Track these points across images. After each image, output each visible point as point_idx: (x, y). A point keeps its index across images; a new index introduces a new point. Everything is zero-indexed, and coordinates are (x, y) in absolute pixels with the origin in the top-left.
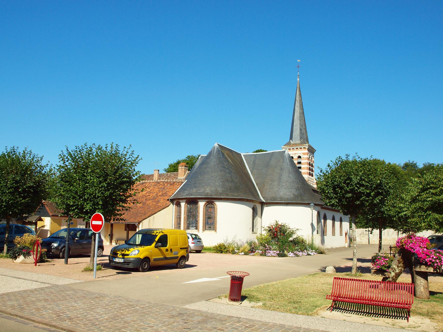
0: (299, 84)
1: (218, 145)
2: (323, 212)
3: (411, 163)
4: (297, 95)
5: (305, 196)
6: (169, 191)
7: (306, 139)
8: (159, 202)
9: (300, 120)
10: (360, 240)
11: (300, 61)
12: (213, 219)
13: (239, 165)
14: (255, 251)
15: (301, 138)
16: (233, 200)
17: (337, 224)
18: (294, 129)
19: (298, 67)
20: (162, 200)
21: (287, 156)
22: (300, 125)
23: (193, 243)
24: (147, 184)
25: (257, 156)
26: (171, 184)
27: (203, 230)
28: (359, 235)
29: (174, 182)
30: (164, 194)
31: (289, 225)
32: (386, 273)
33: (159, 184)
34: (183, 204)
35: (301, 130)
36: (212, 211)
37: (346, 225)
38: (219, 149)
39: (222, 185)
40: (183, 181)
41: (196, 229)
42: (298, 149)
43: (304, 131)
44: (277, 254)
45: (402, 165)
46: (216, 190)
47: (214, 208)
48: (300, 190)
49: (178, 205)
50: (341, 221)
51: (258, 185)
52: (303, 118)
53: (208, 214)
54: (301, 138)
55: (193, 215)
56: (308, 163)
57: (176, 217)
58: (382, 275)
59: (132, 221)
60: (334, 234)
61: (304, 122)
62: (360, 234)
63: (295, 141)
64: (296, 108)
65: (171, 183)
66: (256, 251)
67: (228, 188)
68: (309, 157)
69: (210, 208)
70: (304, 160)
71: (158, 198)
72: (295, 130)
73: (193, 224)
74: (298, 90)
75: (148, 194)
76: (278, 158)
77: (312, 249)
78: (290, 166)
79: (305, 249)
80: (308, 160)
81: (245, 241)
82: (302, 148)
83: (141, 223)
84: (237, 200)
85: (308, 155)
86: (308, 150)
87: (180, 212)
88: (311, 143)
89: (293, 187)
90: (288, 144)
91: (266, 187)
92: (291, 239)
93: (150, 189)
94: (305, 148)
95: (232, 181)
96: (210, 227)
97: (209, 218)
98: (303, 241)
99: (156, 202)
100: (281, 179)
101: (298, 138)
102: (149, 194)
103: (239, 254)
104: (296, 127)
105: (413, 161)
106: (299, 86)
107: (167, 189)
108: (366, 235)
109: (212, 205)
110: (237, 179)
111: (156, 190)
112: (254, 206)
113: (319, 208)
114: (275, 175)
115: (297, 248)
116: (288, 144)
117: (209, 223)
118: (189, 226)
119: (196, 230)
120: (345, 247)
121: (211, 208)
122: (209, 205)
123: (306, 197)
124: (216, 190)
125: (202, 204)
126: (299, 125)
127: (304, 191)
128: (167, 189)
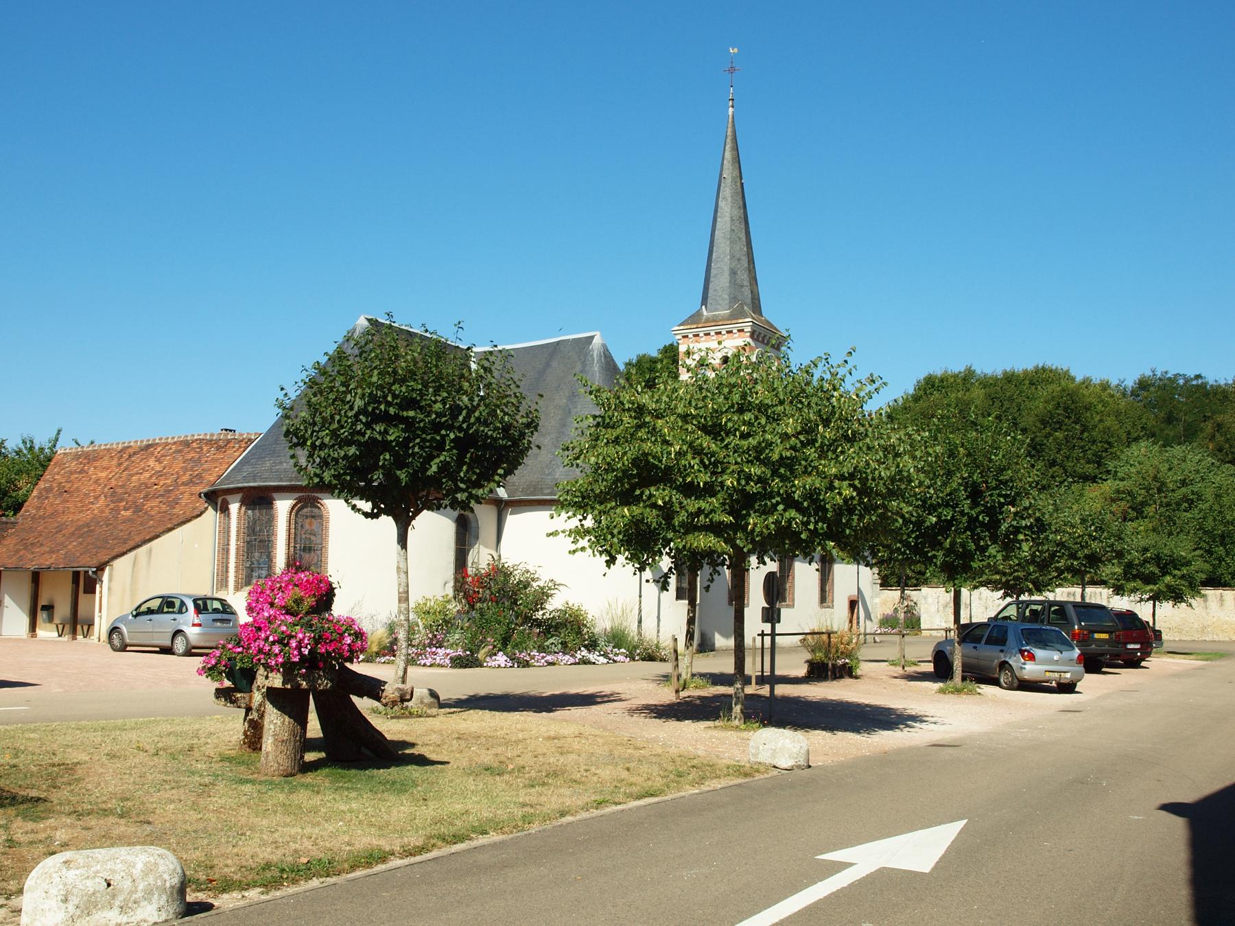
0: (733, 126)
3: (1160, 379)
6: (209, 470)
7: (749, 301)
8: (177, 503)
9: (731, 242)
11: (736, 50)
12: (319, 553)
15: (734, 298)
19: (732, 70)
20: (187, 495)
22: (731, 259)
23: (200, 625)
24: (159, 449)
26: (219, 448)
28: (941, 608)
29: (229, 441)
32: (239, 695)
33: (189, 446)
34: (234, 508)
35: (733, 273)
36: (314, 527)
40: (253, 437)
43: (743, 277)
45: (1130, 383)
47: (321, 517)
49: (224, 509)
52: (743, 236)
54: (734, 299)
55: (260, 541)
57: (223, 549)
58: (226, 700)
59: (81, 563)
63: (716, 310)
65: (221, 443)
69: (308, 521)
71: (178, 490)
72: (716, 276)
73: (262, 568)
74: (728, 147)
75: (154, 480)
76: (569, 359)
82: (735, 331)
87: (226, 531)
88: (773, 313)
90: (695, 319)
93: (162, 463)
94: (742, 330)
99: (170, 502)
101: (724, 299)
102: (157, 478)
105: (1166, 373)
106: (734, 132)
107: (206, 461)
109: (316, 510)
111: (178, 465)
116: (695, 319)
121: (313, 517)
122: (305, 510)
125: (283, 506)
128: (206, 461)
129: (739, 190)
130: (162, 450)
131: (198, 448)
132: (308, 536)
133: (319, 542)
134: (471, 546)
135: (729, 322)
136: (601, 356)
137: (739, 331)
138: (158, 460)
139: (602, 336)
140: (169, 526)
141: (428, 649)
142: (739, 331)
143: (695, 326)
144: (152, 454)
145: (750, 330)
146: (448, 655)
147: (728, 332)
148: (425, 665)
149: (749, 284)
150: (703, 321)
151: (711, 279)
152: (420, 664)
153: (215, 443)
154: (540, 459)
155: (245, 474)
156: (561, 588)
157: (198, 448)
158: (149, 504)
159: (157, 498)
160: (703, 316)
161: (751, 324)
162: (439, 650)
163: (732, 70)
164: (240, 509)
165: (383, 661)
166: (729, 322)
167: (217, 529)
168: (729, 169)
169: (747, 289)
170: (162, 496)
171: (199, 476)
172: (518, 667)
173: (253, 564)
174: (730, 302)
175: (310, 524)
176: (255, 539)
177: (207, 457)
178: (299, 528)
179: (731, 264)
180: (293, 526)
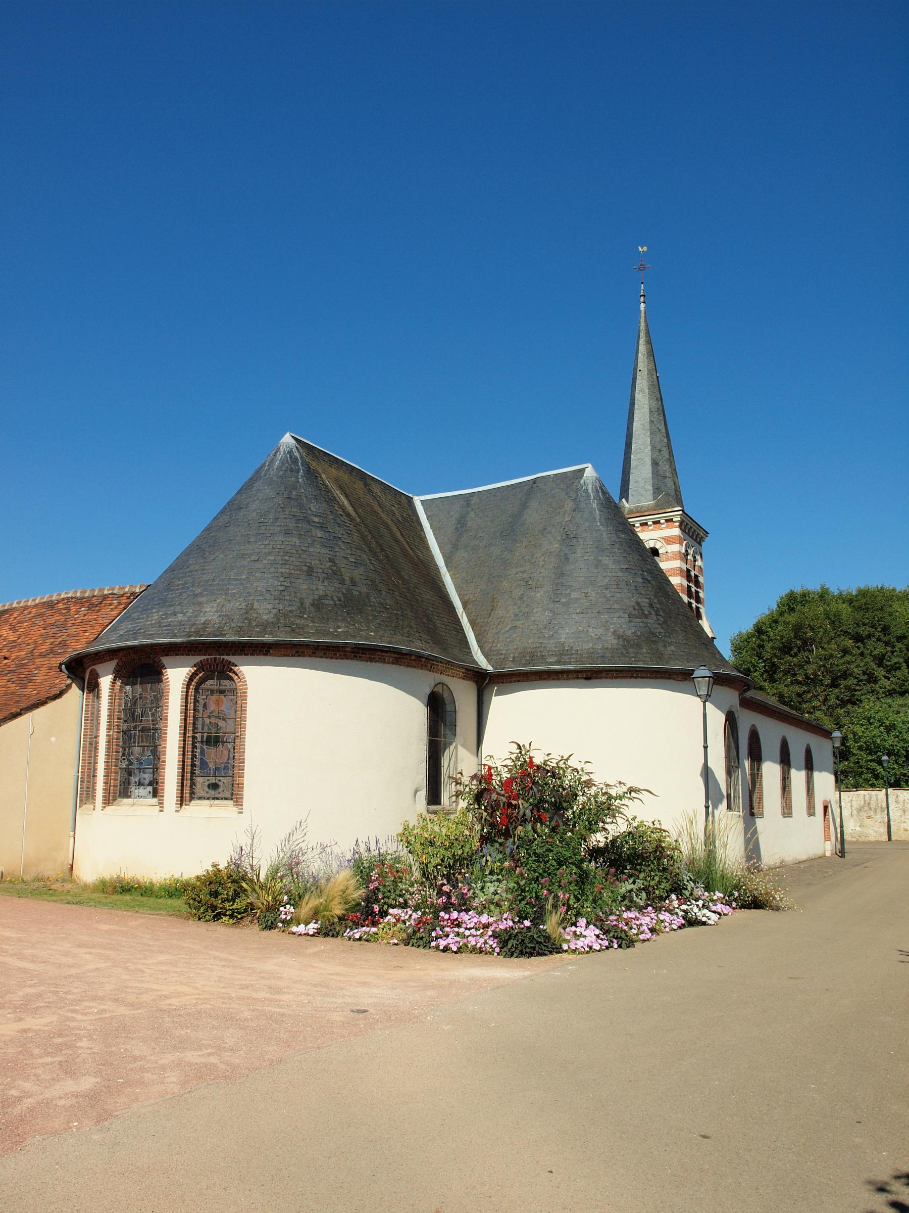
1: (293, 441)
2: (747, 720)
4: (640, 355)
5: (671, 644)
7: (672, 492)
8: (31, 681)
9: (651, 433)
10: (858, 829)
11: (645, 249)
12: (230, 746)
13: (394, 528)
14: (384, 914)
15: (658, 489)
16: (325, 656)
17: (798, 777)
18: (633, 463)
20: (43, 670)
21: (590, 487)
22: (652, 450)
25: (474, 500)
27: (181, 801)
28: (855, 812)
30: (56, 646)
31: (588, 769)
34: (105, 682)
35: (655, 463)
36: (223, 707)
37: (824, 781)
38: (297, 454)
39: (281, 588)
41: (155, 794)
42: (646, 524)
43: (665, 468)
44: (495, 935)
46: (250, 608)
47: (234, 691)
48: (646, 617)
49: (93, 687)
50: (809, 766)
51: (470, 606)
52: (662, 427)
53: (207, 721)
54: (657, 490)
55: (142, 730)
56: (681, 569)
57: (91, 744)
60: (787, 811)
61: (665, 440)
62: (860, 810)
64: (638, 396)
65: (94, 600)
66: (391, 911)
67: (307, 602)
68: (686, 551)
69: (214, 698)
70: (668, 560)
72: (636, 467)
77: (708, 888)
78: (602, 524)
79: (672, 891)
80: (681, 559)
81: (345, 849)
84: (346, 657)
85: (681, 544)
86: (680, 526)
87: (93, 718)
89: (616, 606)
91: (500, 612)
92: (598, 839)
94: (671, 520)
95: (335, 574)
96: (214, 786)
97: (214, 741)
98: (659, 851)
100: (562, 574)
101: (646, 490)
103: (294, 929)
104: (639, 456)
107: (73, 625)
108: (879, 811)
109: (226, 683)
110: (361, 570)
112: (439, 689)
113: (731, 697)
114: (541, 563)
115: (625, 887)
117: (212, 766)
118: (129, 784)
120: (824, 856)
121: (222, 692)
122: (209, 682)
123: (673, 648)
124: (250, 608)
127: (665, 622)
128: (73, 625)
129: (656, 382)
130: (19, 615)
131: (65, 609)
132: (213, 721)
133: (230, 729)
135: (656, 512)
136: (597, 491)
137: (667, 521)
138: (13, 629)
139: (595, 468)
140: (14, 710)
141: (442, 914)
142: (667, 521)
144: (7, 621)
146: (486, 926)
147: (654, 523)
148: (446, 949)
149: (671, 475)
151: (631, 471)
152: (437, 947)
153: (86, 602)
154: (533, 619)
155: (122, 633)
156: (644, 796)
157: (65, 609)
159: (6, 675)
160: (625, 508)
161: (681, 512)
162: (465, 917)
163: (642, 268)
164: (113, 683)
166: (656, 512)
167: (84, 715)
168: (644, 362)
169: (670, 480)
170: (12, 672)
171: (63, 644)
172: (620, 946)
174: (654, 493)
175: (218, 703)
176: (135, 727)
179: (652, 454)
180: (191, 706)
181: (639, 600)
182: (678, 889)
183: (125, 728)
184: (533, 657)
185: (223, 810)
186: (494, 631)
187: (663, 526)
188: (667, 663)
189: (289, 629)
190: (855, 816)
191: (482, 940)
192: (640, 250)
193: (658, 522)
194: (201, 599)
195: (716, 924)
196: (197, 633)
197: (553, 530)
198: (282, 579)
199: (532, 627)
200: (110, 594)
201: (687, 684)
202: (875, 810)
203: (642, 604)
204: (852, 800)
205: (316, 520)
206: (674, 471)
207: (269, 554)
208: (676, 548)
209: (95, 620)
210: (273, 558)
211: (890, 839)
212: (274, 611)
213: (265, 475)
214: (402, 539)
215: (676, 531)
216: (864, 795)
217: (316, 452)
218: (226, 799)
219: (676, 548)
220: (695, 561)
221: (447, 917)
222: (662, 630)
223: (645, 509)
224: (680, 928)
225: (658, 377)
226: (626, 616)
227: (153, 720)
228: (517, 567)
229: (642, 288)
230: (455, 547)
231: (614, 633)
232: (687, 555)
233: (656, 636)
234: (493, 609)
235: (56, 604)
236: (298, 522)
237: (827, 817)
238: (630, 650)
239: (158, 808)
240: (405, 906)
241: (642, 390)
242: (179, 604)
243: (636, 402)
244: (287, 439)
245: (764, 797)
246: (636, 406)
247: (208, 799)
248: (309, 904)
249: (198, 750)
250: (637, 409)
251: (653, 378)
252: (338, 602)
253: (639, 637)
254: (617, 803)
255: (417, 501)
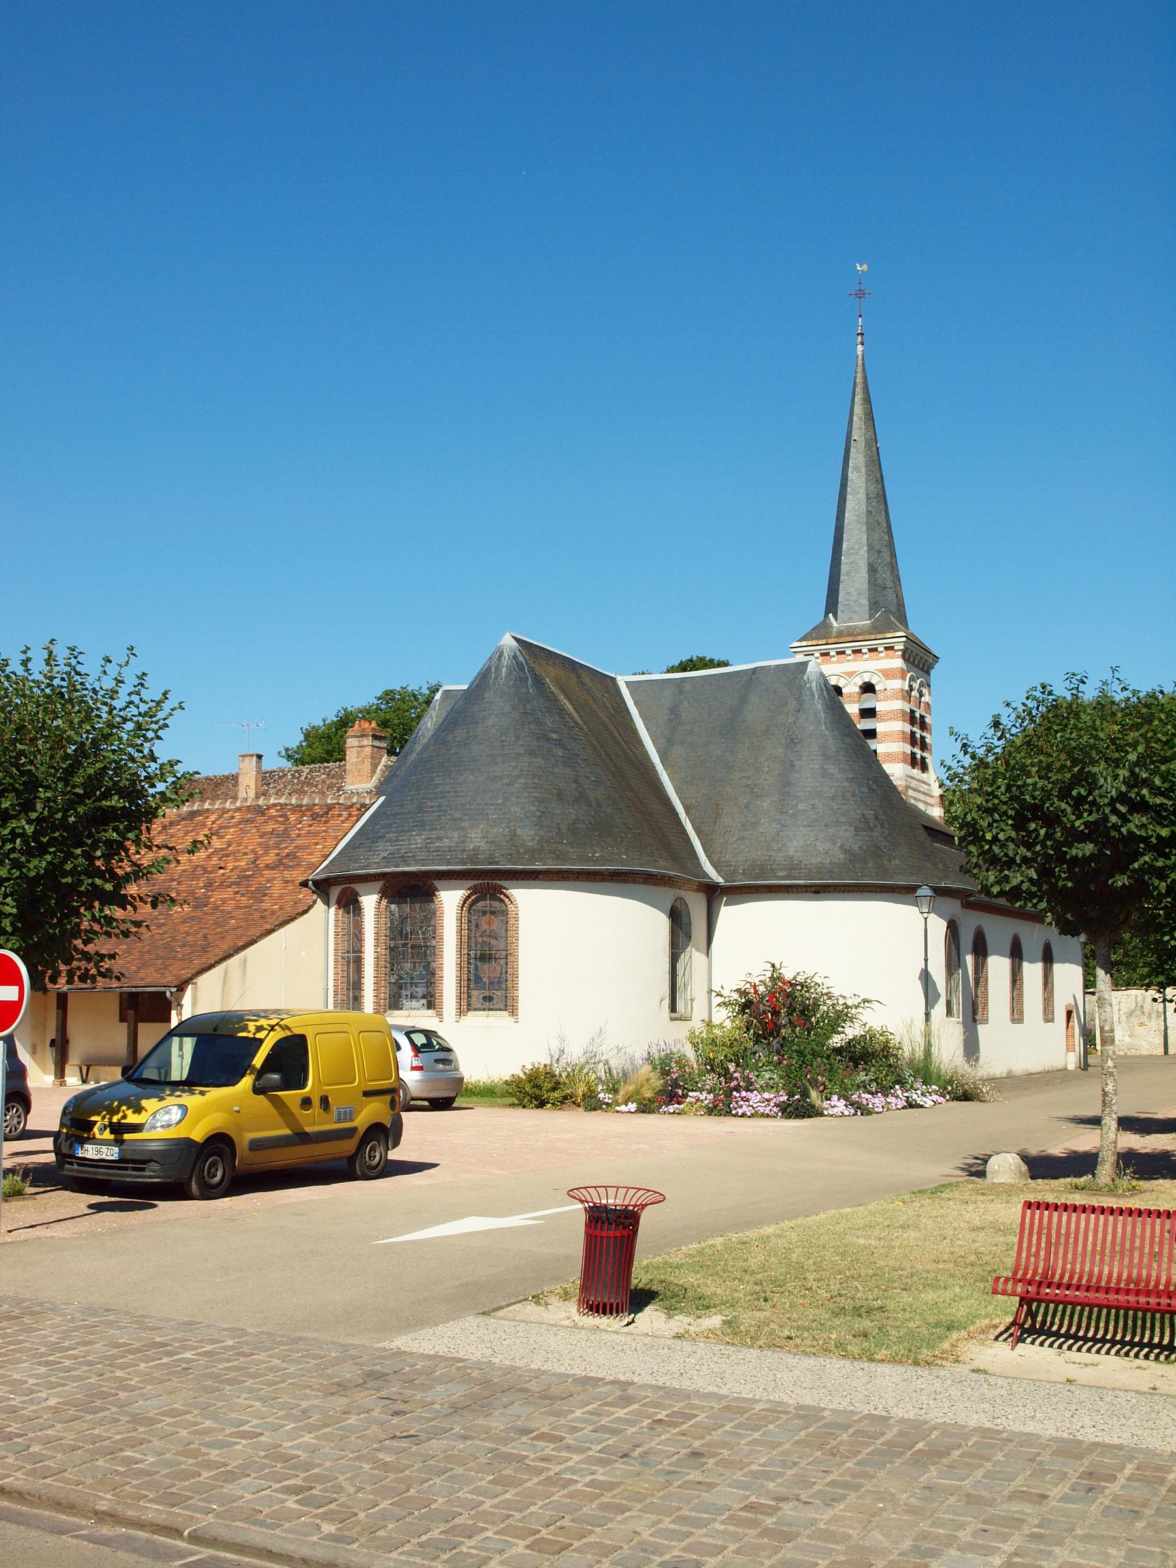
0: (864, 370)
1: (515, 643)
2: (970, 922)
4: (855, 418)
5: (894, 858)
6: (307, 847)
7: (894, 608)
8: (265, 895)
9: (868, 528)
10: (1127, 1039)
11: (865, 267)
12: (502, 962)
14: (685, 1096)
18: (844, 568)
19: (860, 294)
20: (278, 884)
22: (869, 551)
24: (213, 818)
26: (315, 817)
27: (461, 1012)
29: (330, 808)
33: (263, 814)
34: (369, 902)
35: (872, 569)
36: (494, 927)
38: (521, 659)
39: (538, 814)
40: (367, 802)
41: (430, 1005)
42: (859, 651)
43: (885, 575)
44: (776, 1105)
46: (513, 834)
47: (505, 913)
48: (872, 830)
49: (350, 904)
52: (882, 519)
53: (480, 940)
54: (874, 606)
55: (413, 947)
56: (903, 711)
57: (343, 958)
59: (148, 981)
60: (1017, 1015)
61: (886, 537)
62: (1130, 1015)
63: (850, 619)
64: (851, 475)
65: (317, 809)
66: (690, 1094)
67: (564, 827)
68: (910, 686)
70: (886, 699)
72: (847, 574)
73: (416, 985)
74: (858, 399)
75: (215, 861)
78: (827, 728)
80: (904, 699)
82: (881, 649)
83: (190, 989)
85: (904, 678)
86: (903, 656)
89: (843, 819)
90: (820, 632)
91: (725, 820)
92: (836, 1041)
93: (223, 837)
94: (892, 648)
95: (581, 798)
96: (488, 999)
99: (252, 892)
100: (788, 784)
101: (861, 606)
103: (618, 1108)
104: (851, 559)
106: (865, 378)
107: (299, 836)
108: (1154, 1016)
109: (496, 904)
111: (252, 841)
112: (678, 904)
113: (954, 906)
114: (766, 769)
115: (862, 1077)
116: (820, 632)
117: (485, 980)
118: (400, 997)
119: (430, 1012)
120: (1066, 1069)
121: (493, 913)
122: (481, 904)
124: (513, 834)
126: (866, 548)
128: (299, 836)
131: (280, 816)
133: (502, 947)
134: (684, 950)
136: (821, 688)
140: (268, 927)
142: (886, 649)
143: (824, 642)
145: (902, 647)
147: (870, 650)
148: (743, 1115)
149: (892, 585)
150: (834, 634)
153: (308, 810)
156: (875, 1005)
158: (216, 897)
159: (229, 886)
161: (904, 639)
165: (671, 1111)
166: (873, 637)
168: (861, 428)
169: (891, 591)
170: (238, 884)
173: (401, 978)
177: (299, 829)
178: (473, 928)
179: (868, 558)
180: (465, 926)
181: (865, 812)
182: (900, 1081)
183: (392, 945)
184: (763, 869)
185: (498, 1020)
186: (722, 840)
187: (881, 655)
188: (891, 879)
189: (554, 856)
190: (1123, 1023)
191: (768, 1108)
192: (858, 268)
193: (875, 650)
194: (463, 824)
195: (931, 1107)
196: (471, 860)
197: (777, 732)
198: (536, 804)
199: (760, 839)
200: (335, 804)
201: (910, 897)
202: (1150, 1014)
203: (868, 816)
204: (1120, 1002)
205: (554, 736)
206: (896, 578)
207: (518, 777)
208: (898, 684)
209: (324, 831)
210: (524, 781)
211: (1166, 1052)
212: (537, 838)
213: (494, 684)
214: (619, 738)
215: (898, 663)
216: (1136, 996)
217: (533, 649)
218: (500, 1010)
219: (898, 684)
220: (921, 696)
221: (738, 1095)
222: (887, 843)
223: (859, 631)
224: (903, 1108)
225: (878, 449)
226: (852, 829)
227: (424, 939)
228: (740, 771)
229: (860, 323)
230: (670, 741)
231: (841, 847)
232: (911, 689)
233: (881, 850)
234: (718, 816)
235: (268, 809)
236: (538, 739)
237: (1071, 1024)
238: (857, 865)
239: (437, 1019)
240: (701, 1090)
241: (856, 468)
242: (441, 829)
243: (849, 483)
244: (507, 641)
245: (989, 1002)
246: (849, 489)
247: (484, 1010)
248: (625, 1090)
249: (473, 966)
250: (851, 494)
251: (871, 452)
252: (589, 826)
253: (865, 851)
254: (853, 1011)
255: (621, 681)
